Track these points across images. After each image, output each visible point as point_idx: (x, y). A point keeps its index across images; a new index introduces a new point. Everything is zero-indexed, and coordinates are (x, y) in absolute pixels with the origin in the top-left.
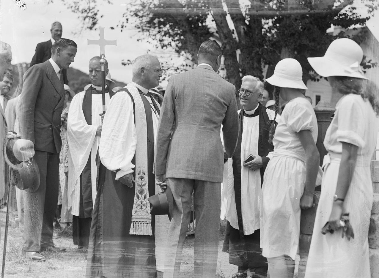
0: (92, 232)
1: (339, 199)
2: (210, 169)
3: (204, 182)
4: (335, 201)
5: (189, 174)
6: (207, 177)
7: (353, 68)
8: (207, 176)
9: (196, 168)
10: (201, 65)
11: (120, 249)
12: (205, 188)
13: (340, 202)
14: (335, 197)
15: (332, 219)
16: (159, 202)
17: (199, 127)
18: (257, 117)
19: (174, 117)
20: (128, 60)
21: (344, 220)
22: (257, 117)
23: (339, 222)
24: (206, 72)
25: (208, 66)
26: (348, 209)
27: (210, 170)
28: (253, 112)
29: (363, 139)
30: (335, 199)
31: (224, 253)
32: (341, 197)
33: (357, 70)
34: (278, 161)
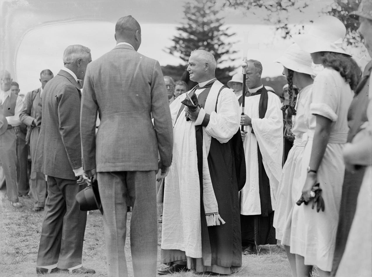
0: (128, 222)
1: (311, 171)
2: (138, 158)
3: (133, 173)
4: (309, 172)
5: (115, 166)
6: (136, 166)
7: (336, 44)
8: (137, 165)
9: (41, 166)
10: (121, 45)
11: (197, 229)
12: (135, 178)
13: (312, 173)
14: (308, 169)
15: (305, 190)
16: (84, 198)
17: (122, 114)
18: (259, 96)
19: (300, 95)
20: (357, 47)
21: (314, 190)
22: (259, 96)
23: (310, 192)
24: (122, 52)
25: (125, 45)
26: (320, 180)
27: (139, 159)
28: (255, 90)
29: (336, 113)
30: (309, 171)
31: (48, 269)
32: (313, 169)
33: (341, 46)
34: (183, 147)
